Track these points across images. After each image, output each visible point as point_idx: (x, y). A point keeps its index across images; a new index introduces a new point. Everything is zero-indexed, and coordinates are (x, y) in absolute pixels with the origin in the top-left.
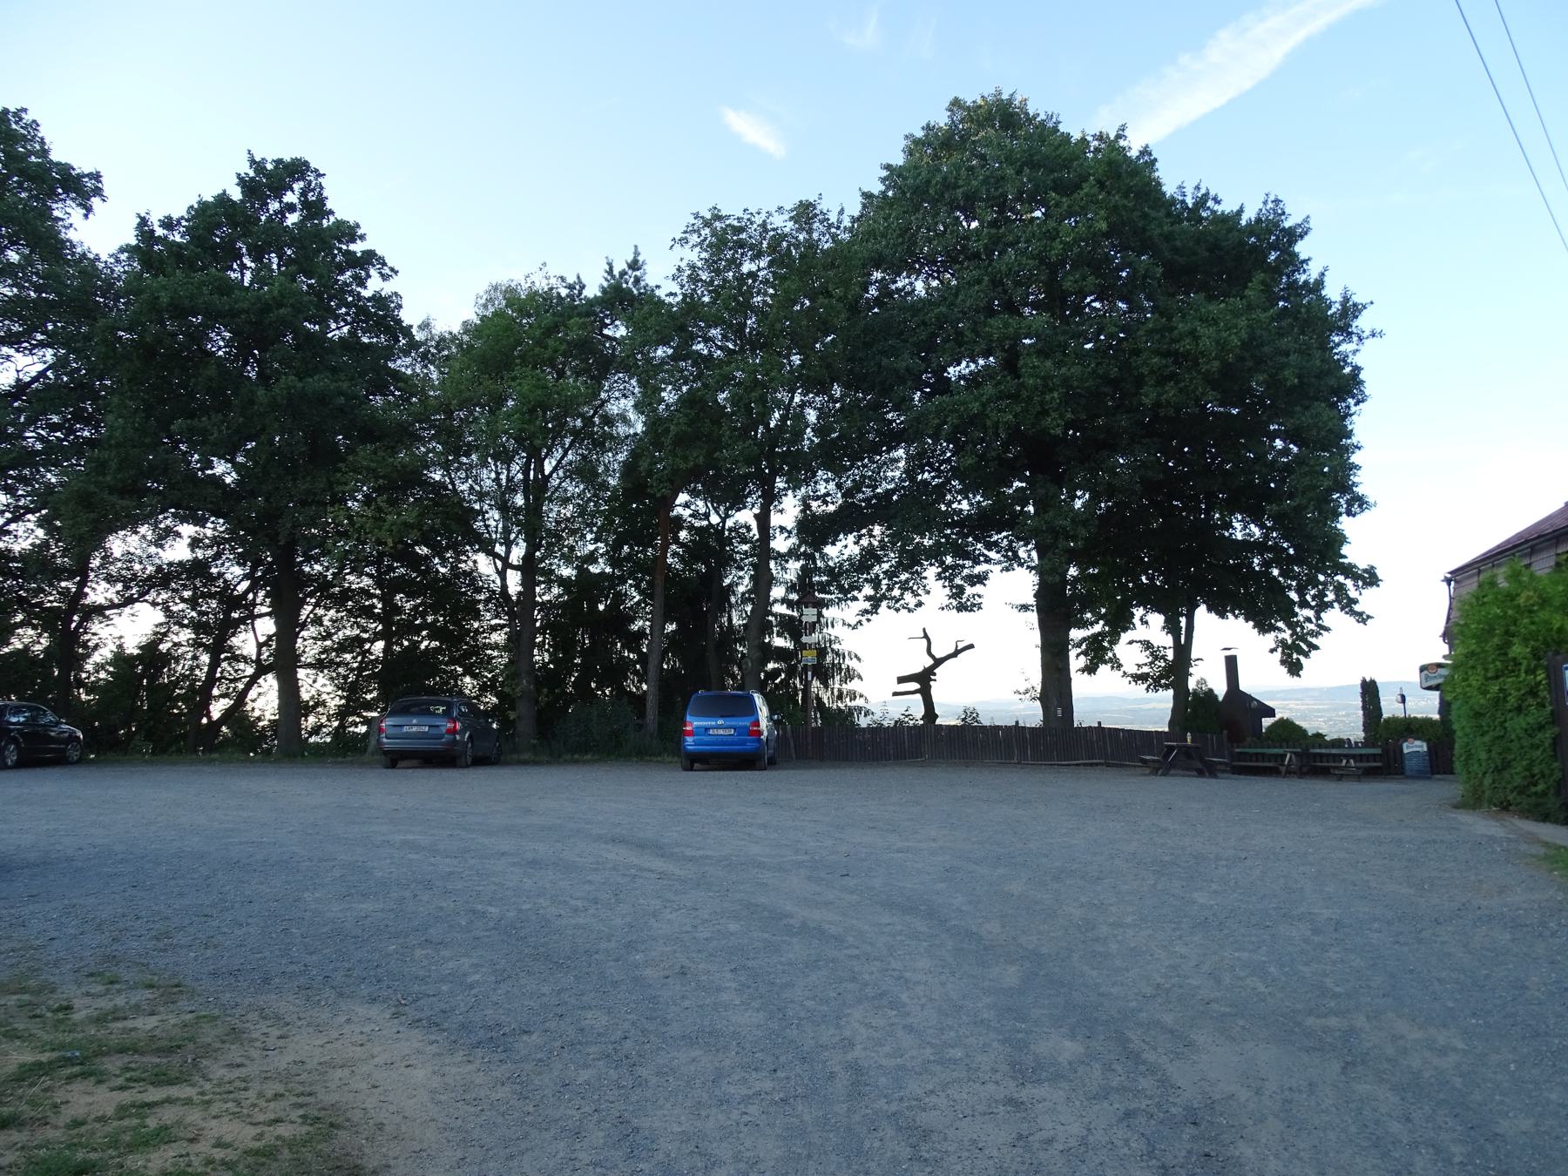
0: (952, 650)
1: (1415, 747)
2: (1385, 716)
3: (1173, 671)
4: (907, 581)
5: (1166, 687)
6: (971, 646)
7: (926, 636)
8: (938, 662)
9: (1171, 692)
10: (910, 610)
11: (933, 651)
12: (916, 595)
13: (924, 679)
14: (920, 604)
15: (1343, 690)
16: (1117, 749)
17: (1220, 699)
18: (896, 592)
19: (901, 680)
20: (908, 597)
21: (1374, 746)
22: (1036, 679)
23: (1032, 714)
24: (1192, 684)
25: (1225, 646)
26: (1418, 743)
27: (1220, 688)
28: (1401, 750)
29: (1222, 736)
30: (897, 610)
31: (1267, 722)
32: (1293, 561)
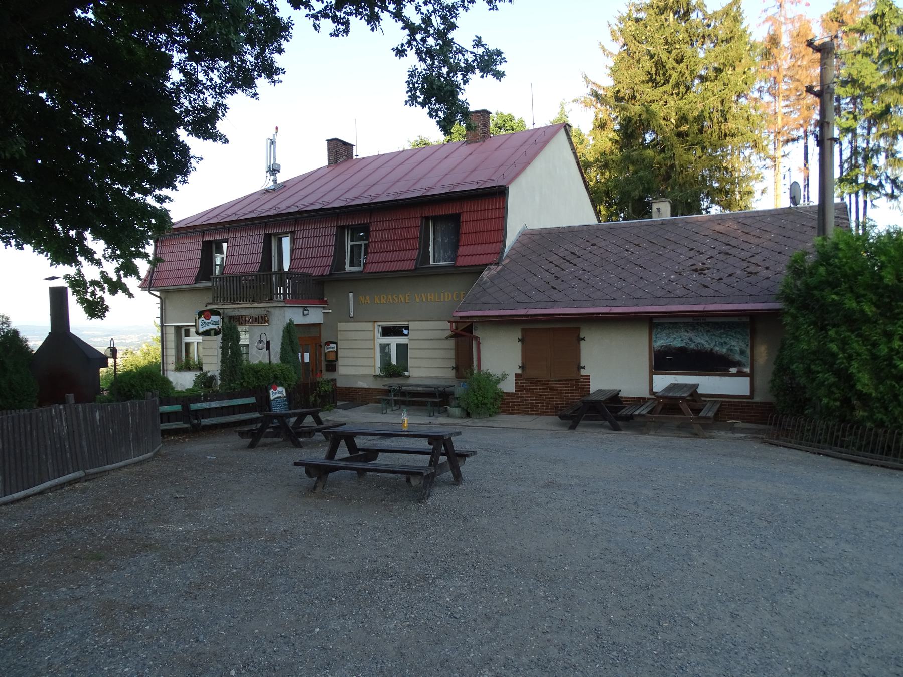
23: (749, 378)
26: (280, 389)
28: (268, 396)
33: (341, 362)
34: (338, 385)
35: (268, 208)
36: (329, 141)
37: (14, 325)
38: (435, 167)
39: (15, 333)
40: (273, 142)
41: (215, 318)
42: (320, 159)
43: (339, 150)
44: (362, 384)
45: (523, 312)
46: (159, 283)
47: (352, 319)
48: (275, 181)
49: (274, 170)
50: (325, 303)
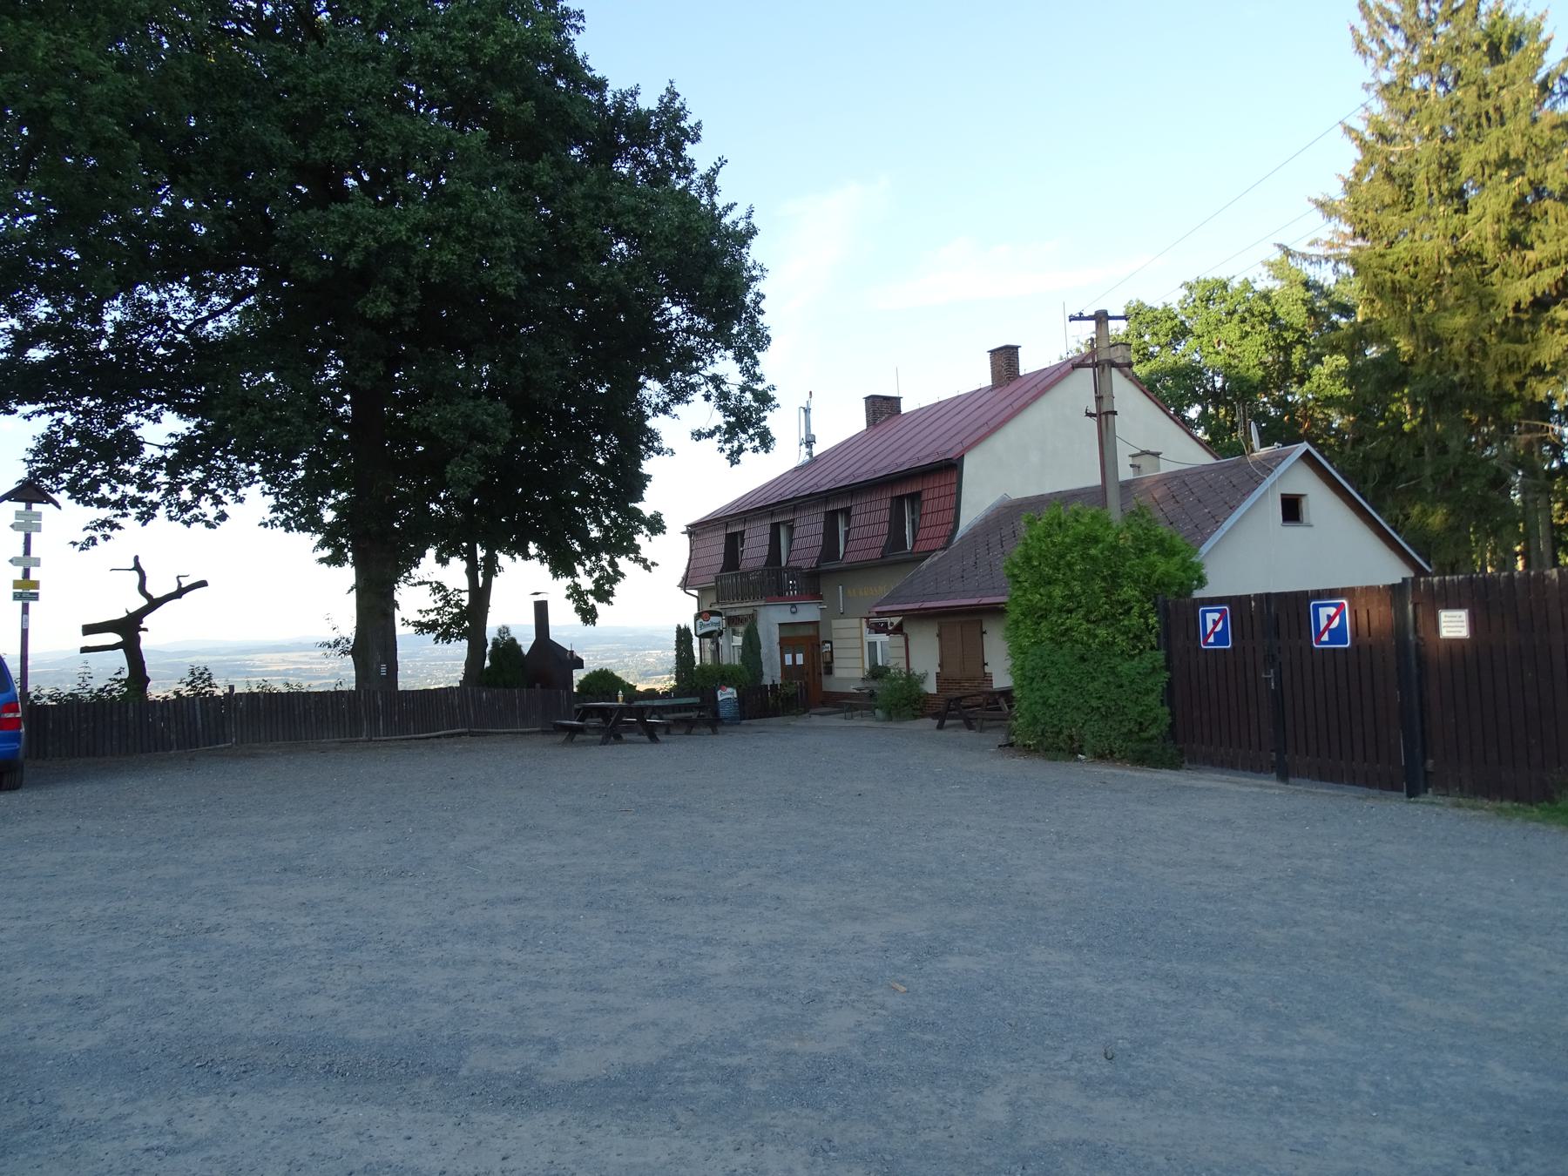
0: (174, 588)
1: (727, 694)
2: (737, 662)
3: (467, 619)
4: (204, 482)
5: (460, 637)
6: (203, 584)
7: (137, 567)
8: (154, 604)
9: (465, 643)
10: (209, 525)
11: (149, 589)
12: (218, 501)
13: (129, 627)
14: (223, 517)
15: (649, 641)
16: (429, 714)
17: (526, 651)
18: (186, 495)
19: (89, 630)
20: (206, 505)
21: (690, 695)
22: (348, 627)
23: (340, 674)
24: (491, 632)
25: (522, 591)
26: (730, 690)
27: (526, 641)
28: (716, 697)
29: (529, 690)
30: (188, 523)
31: (578, 675)
32: (574, 500)
33: (836, 663)
34: (404, 684)
35: (806, 486)
36: (867, 399)
37: (513, 634)
38: (25, 633)
39: (514, 640)
40: (807, 411)
41: (714, 619)
42: (857, 422)
43: (882, 408)
44: (852, 689)
45: (917, 606)
46: (699, 580)
47: (842, 615)
48: (810, 454)
49: (809, 442)
50: (821, 597)
